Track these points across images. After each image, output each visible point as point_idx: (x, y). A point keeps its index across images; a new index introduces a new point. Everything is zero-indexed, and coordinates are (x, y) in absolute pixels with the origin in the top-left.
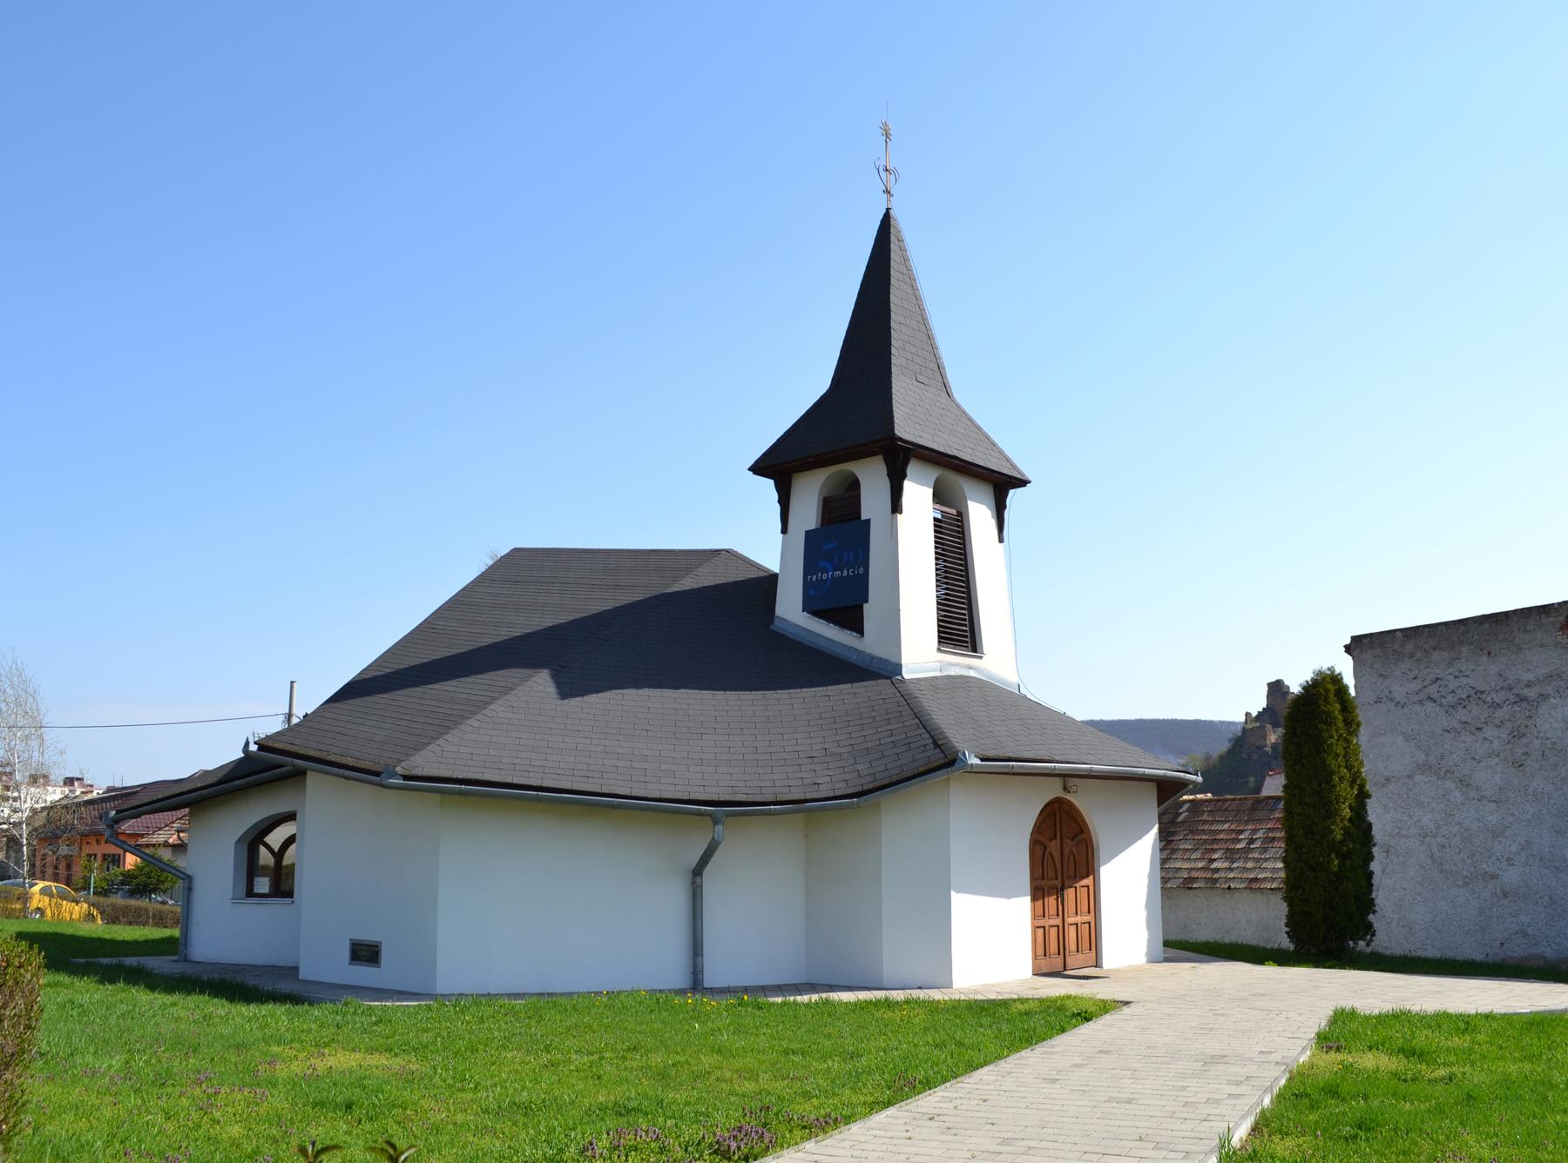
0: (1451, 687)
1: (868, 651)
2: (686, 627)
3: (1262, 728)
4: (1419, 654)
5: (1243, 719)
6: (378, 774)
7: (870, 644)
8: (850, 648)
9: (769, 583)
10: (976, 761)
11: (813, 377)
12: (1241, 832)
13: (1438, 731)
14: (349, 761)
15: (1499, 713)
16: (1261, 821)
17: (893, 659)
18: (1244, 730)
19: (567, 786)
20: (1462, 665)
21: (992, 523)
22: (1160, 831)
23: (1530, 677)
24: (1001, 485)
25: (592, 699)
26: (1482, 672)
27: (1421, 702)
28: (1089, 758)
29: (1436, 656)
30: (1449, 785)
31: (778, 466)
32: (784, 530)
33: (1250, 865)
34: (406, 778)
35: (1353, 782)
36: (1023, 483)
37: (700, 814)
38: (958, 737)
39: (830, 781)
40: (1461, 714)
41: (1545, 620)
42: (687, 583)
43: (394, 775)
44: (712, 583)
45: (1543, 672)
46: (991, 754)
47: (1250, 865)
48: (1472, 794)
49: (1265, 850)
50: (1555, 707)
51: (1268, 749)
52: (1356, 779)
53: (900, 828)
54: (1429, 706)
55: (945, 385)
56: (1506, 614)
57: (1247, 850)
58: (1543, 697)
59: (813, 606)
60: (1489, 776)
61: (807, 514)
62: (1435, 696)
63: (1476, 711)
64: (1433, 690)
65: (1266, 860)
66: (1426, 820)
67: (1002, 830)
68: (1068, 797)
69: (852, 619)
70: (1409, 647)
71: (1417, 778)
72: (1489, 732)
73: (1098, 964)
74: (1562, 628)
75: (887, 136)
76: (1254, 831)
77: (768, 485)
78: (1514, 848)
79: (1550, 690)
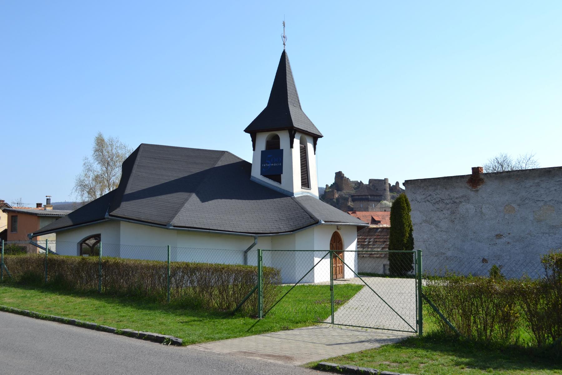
0: (434, 197)
1: (283, 188)
2: (219, 177)
3: (333, 191)
4: (425, 187)
5: (325, 187)
6: (165, 225)
7: (283, 186)
8: (277, 187)
9: (246, 166)
10: (323, 222)
11: (260, 102)
12: (366, 239)
13: (430, 211)
14: (150, 221)
15: (448, 206)
16: (372, 235)
17: (291, 191)
18: (325, 192)
19: (216, 229)
20: (438, 191)
21: (313, 149)
22: (358, 242)
23: (457, 196)
24: (315, 137)
25: (210, 202)
26: (443, 194)
27: (425, 202)
28: (347, 221)
29: (430, 188)
30: (432, 226)
31: (253, 130)
32: (254, 150)
33: (369, 249)
34: (174, 226)
35: (409, 226)
36: (321, 137)
37: (251, 236)
38: (317, 215)
39: (283, 227)
40: (437, 206)
41: (462, 180)
42: (220, 164)
43: (171, 225)
44: (227, 164)
45: (461, 195)
46: (326, 220)
47: (369, 249)
48: (439, 229)
49: (374, 245)
50: (464, 205)
51: (335, 200)
52: (410, 226)
53: (301, 241)
54: (428, 203)
55: (300, 106)
56: (451, 177)
57: (368, 245)
58: (461, 202)
59: (264, 173)
60: (444, 224)
61: (262, 145)
62: (430, 200)
63: (441, 205)
64: (429, 198)
65: (375, 248)
66: (425, 237)
67: (321, 240)
68: (338, 231)
69: (277, 178)
70: (422, 185)
71: (423, 224)
72: (445, 211)
73: (343, 278)
74: (467, 182)
75: (284, 25)
76: (370, 239)
77: (248, 135)
78: (450, 246)
79: (463, 200)
